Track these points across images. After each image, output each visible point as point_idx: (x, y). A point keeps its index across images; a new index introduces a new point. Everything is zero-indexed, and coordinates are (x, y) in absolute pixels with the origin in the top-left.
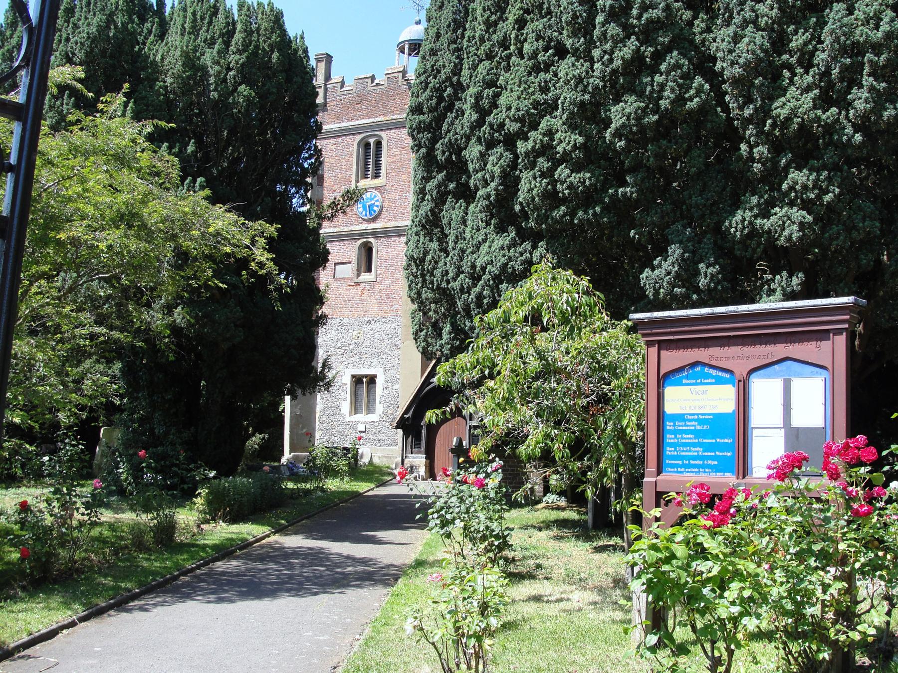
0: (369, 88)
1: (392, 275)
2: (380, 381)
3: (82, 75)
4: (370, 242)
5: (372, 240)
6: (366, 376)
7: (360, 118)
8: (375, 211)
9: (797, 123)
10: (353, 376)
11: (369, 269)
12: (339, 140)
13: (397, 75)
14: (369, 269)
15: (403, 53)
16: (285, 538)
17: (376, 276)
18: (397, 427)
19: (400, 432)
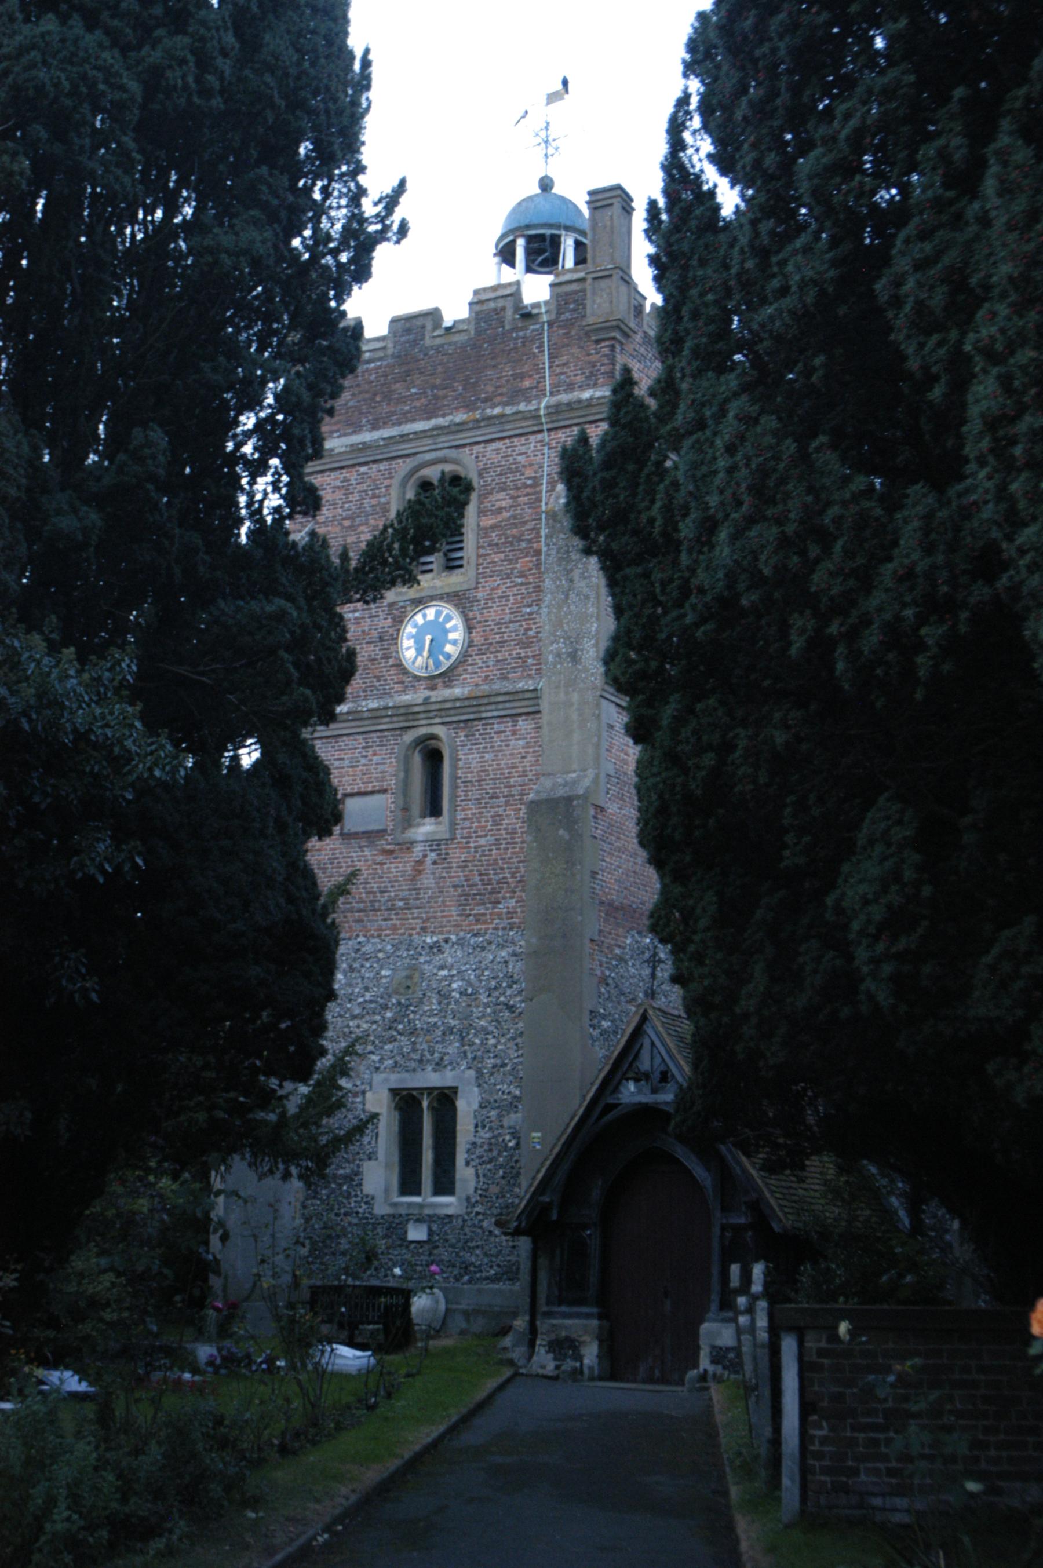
0: (428, 342)
1: (497, 820)
2: (466, 1106)
3: (311, 147)
4: (434, 737)
5: (440, 731)
6: (430, 1090)
7: (406, 418)
8: (448, 656)
9: (888, 192)
10: (394, 1092)
11: (434, 809)
12: (353, 476)
13: (500, 303)
14: (434, 809)
15: (512, 264)
16: (411, 739)
17: (453, 824)
18: (517, 1232)
19: (524, 1243)
